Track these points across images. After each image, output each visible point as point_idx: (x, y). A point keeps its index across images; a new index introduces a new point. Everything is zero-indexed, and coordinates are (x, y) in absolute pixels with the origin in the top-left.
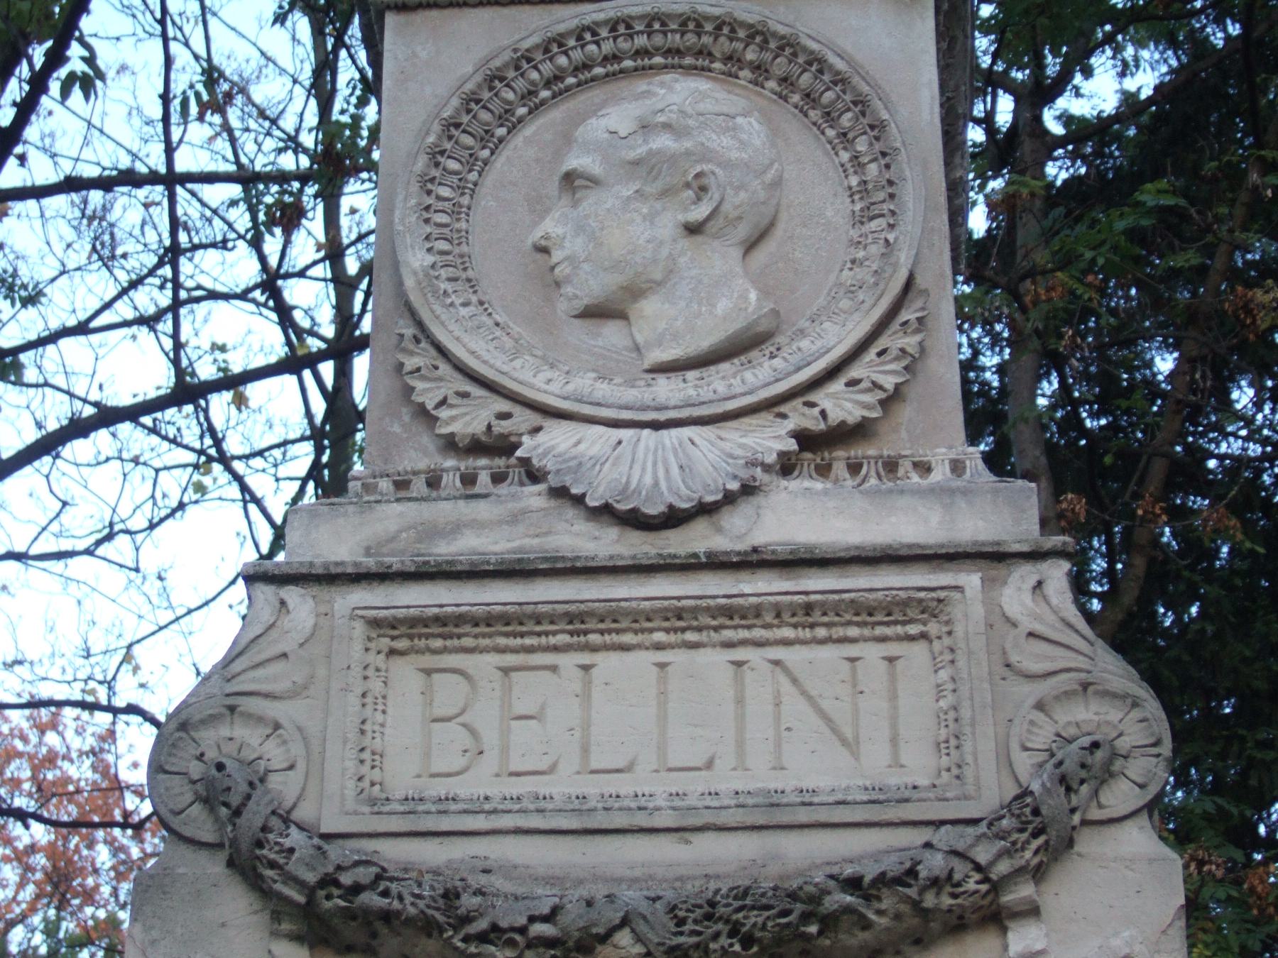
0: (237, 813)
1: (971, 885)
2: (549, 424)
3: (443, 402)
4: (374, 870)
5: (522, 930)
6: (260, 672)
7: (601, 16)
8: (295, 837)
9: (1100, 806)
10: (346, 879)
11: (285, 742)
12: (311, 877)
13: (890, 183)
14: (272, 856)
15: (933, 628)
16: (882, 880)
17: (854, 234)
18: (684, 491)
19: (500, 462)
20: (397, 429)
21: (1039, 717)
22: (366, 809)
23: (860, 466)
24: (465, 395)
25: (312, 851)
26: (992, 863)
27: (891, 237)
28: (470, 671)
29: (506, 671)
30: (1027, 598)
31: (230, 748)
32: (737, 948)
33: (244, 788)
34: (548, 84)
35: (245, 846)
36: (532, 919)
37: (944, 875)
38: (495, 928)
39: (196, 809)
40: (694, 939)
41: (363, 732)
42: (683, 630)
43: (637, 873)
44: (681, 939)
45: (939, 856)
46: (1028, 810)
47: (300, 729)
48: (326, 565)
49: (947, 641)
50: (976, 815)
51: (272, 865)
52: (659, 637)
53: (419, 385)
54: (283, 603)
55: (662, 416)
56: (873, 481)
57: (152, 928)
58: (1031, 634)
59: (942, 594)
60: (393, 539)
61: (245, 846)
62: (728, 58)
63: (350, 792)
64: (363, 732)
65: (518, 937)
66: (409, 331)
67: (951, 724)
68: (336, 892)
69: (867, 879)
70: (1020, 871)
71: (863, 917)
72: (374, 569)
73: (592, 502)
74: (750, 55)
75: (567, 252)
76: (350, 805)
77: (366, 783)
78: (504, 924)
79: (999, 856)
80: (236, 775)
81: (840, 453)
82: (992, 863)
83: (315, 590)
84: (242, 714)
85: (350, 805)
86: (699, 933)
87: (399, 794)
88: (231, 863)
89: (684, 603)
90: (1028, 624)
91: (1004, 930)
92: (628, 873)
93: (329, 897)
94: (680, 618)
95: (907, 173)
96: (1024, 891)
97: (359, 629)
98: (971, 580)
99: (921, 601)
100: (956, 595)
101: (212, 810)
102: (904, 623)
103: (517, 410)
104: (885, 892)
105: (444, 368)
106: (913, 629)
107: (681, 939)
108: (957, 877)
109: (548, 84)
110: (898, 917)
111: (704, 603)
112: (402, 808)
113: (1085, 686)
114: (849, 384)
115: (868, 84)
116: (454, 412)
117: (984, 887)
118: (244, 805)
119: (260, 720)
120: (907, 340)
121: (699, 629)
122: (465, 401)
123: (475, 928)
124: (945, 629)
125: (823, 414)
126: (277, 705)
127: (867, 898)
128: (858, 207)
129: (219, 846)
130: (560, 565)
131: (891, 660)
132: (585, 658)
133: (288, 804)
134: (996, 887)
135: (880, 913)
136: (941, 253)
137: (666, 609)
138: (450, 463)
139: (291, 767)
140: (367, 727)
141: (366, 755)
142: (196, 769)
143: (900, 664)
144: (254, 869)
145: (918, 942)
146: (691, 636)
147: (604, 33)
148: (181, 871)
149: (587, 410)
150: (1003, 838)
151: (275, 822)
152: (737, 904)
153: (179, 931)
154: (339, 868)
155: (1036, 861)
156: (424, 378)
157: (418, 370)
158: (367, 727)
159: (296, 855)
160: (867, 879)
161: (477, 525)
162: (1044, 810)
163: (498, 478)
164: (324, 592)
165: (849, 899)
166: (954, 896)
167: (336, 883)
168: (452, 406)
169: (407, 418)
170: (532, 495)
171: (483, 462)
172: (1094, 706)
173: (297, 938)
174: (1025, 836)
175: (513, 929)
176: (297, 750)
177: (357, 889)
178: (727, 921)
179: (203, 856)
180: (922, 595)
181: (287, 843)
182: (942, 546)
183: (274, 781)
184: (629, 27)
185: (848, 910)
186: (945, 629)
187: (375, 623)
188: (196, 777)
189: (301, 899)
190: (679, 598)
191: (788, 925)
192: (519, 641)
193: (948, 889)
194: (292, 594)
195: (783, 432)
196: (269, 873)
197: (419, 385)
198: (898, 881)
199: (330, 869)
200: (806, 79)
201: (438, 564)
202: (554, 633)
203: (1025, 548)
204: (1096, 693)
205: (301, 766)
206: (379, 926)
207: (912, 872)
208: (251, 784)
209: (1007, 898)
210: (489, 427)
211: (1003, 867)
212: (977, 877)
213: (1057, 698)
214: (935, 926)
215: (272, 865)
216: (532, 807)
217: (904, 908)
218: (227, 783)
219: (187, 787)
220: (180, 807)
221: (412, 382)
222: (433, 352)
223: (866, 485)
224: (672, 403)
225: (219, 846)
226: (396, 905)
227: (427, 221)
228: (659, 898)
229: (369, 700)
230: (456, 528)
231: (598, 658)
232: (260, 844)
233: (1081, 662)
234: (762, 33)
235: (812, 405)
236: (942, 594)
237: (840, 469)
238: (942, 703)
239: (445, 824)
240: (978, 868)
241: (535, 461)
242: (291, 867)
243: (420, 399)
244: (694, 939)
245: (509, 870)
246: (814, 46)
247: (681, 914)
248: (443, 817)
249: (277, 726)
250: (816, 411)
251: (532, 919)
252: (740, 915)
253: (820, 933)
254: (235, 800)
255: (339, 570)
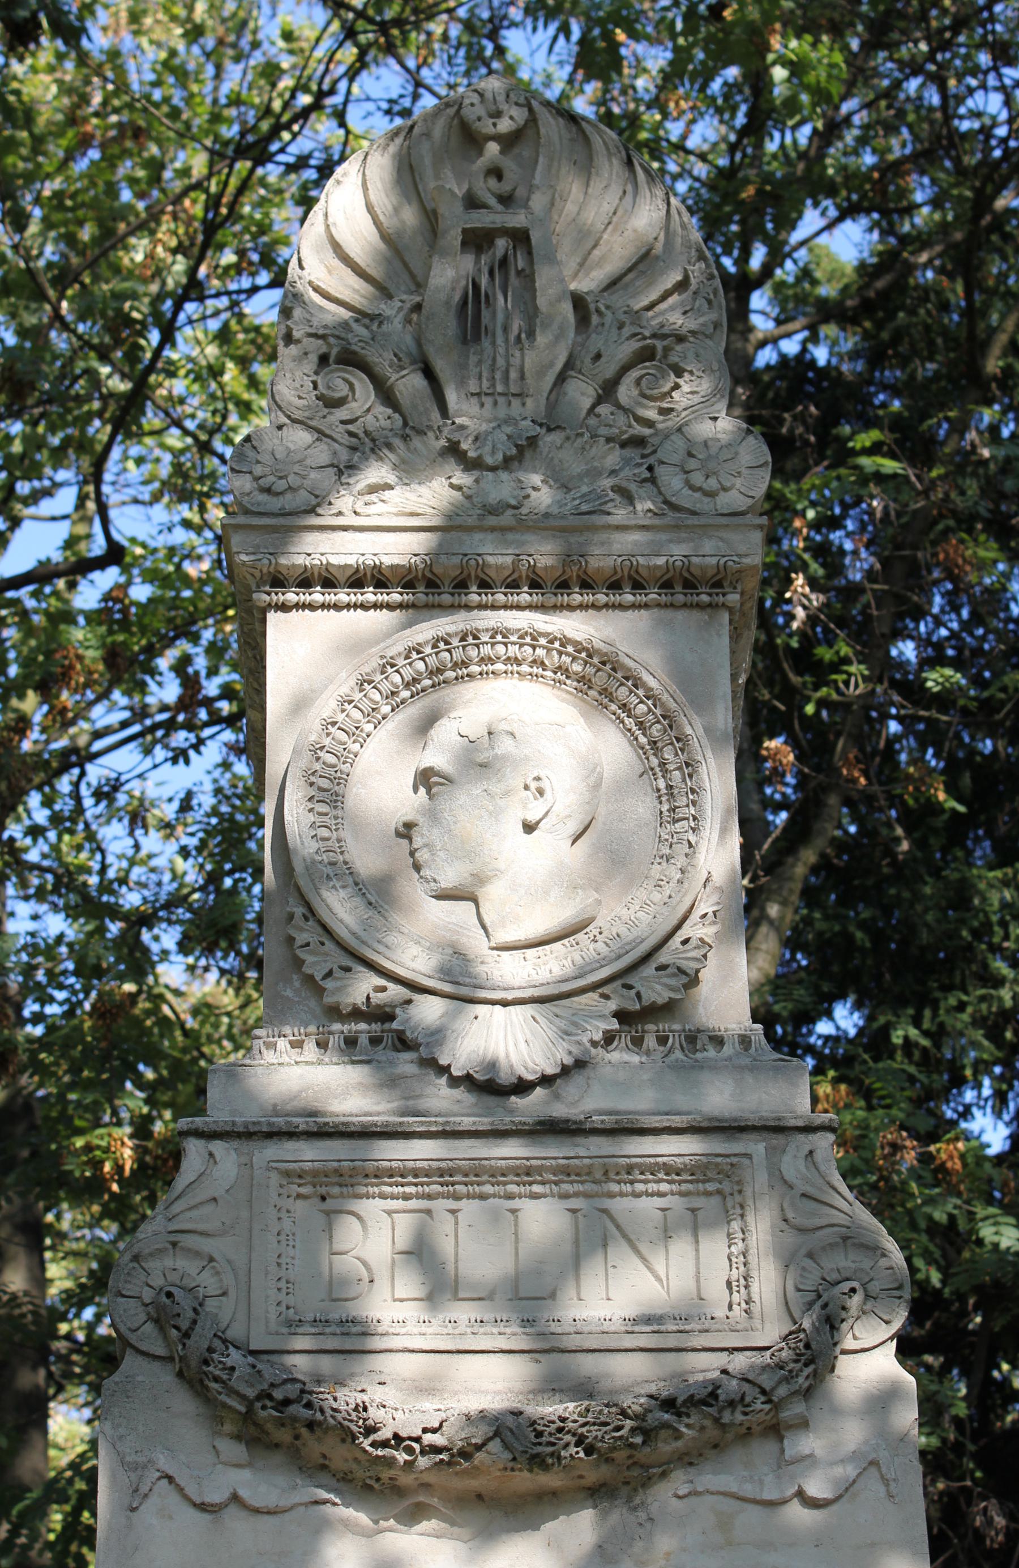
0: (187, 1335)
1: (758, 1406)
2: (417, 997)
3: (330, 974)
4: (298, 1386)
5: (418, 1440)
6: (195, 1213)
7: (451, 629)
8: (235, 1357)
9: (855, 1338)
10: (278, 1394)
11: (218, 1273)
12: (251, 1393)
13: (693, 791)
14: (217, 1373)
16: (692, 1401)
18: (531, 1065)
20: (289, 993)
21: (808, 1263)
22: (285, 1330)
23: (667, 1038)
25: (249, 1370)
26: (773, 1389)
27: (693, 839)
29: (389, 1213)
30: (801, 1164)
31: (173, 1278)
32: (582, 1455)
33: (190, 1314)
34: (407, 685)
35: (194, 1363)
36: (425, 1430)
37: (738, 1398)
38: (396, 1436)
39: (149, 1327)
40: (551, 1449)
41: (279, 1264)
42: (530, 1184)
44: (539, 1449)
45: (734, 1382)
46: (801, 1345)
47: (229, 1262)
48: (246, 1125)
49: (738, 1198)
51: (216, 1379)
52: (513, 1188)
53: (309, 959)
54: (211, 1155)
55: (510, 996)
56: (678, 1054)
57: (119, 1425)
58: (803, 1195)
59: (734, 1160)
61: (194, 1363)
62: (559, 669)
63: (273, 1317)
64: (279, 1264)
65: (416, 1446)
66: (299, 911)
67: (742, 1268)
68: (269, 1404)
69: (680, 1401)
70: (795, 1393)
71: (676, 1430)
72: (285, 1129)
73: (456, 1072)
74: (577, 667)
75: (425, 840)
76: (273, 1327)
77: (283, 1308)
78: (404, 1434)
79: (779, 1383)
80: (183, 1303)
81: (651, 1027)
82: (773, 1389)
83: (235, 1143)
84: (183, 1249)
85: (273, 1327)
86: (553, 1444)
87: (310, 1317)
88: (180, 1374)
89: (534, 1162)
90: (802, 1187)
91: (781, 1439)
93: (264, 1408)
94: (528, 1174)
95: (689, 731)
96: (797, 1408)
97: (275, 1178)
98: (757, 1147)
99: (717, 1164)
100: (746, 1161)
101: (162, 1329)
102: (704, 1182)
103: (391, 986)
104: (693, 1411)
105: (329, 945)
106: (711, 1187)
107: (539, 1449)
108: (748, 1399)
109: (407, 685)
110: (703, 1428)
111: (547, 1163)
112: (313, 1330)
113: (845, 1239)
114: (658, 969)
117: (767, 1407)
118: (192, 1329)
119: (197, 1254)
120: (705, 930)
121: (543, 1183)
123: (378, 1436)
124: (736, 1188)
125: (638, 995)
126: (210, 1241)
127: (679, 1415)
130: (433, 1129)
131: (693, 1210)
132: (452, 1204)
133: (223, 1325)
134: (777, 1406)
135: (688, 1426)
137: (518, 1167)
139: (224, 1294)
140: (283, 1260)
141: (282, 1284)
142: (148, 1295)
143: (700, 1213)
144: (201, 1381)
145: (715, 1446)
146: (537, 1188)
147: (455, 642)
148: (140, 1378)
150: (782, 1368)
151: (217, 1344)
152: (582, 1420)
153: (141, 1428)
154: (272, 1385)
155: (806, 1384)
156: (313, 953)
157: (308, 945)
158: (283, 1260)
159: (237, 1374)
160: (680, 1401)
162: (814, 1345)
163: (375, 1041)
164: (245, 1146)
165: (666, 1416)
166: (745, 1414)
167: (270, 1397)
169: (297, 984)
170: (406, 1062)
171: (363, 1026)
172: (852, 1256)
173: (238, 1437)
174: (799, 1365)
175: (411, 1439)
176: (228, 1280)
177: (287, 1402)
178: (574, 1435)
179: (156, 1365)
180: (719, 1160)
181: (229, 1362)
182: (735, 1120)
183: (211, 1305)
184: (475, 637)
185: (666, 1425)
186: (736, 1188)
187: (287, 1174)
188: (148, 1301)
189: (242, 1409)
190: (528, 1159)
191: (621, 1438)
192: (400, 1189)
193: (740, 1408)
194: (218, 1147)
195: (607, 1012)
196: (213, 1385)
198: (704, 1402)
199: (266, 1386)
200: (623, 692)
201: (336, 1126)
202: (428, 1184)
203: (800, 1123)
204: (854, 1245)
205: (232, 1293)
207: (713, 1395)
208: (195, 1310)
209: (785, 1414)
210: (368, 998)
211: (782, 1391)
212: (763, 1399)
213: (823, 1249)
214: (730, 1436)
215: (216, 1379)
216: (416, 1330)
217: (708, 1423)
218: (176, 1310)
219: (141, 1308)
220: (136, 1325)
221: (301, 954)
222: (320, 930)
223: (672, 1057)
224: (517, 984)
225: (170, 1359)
226: (319, 1416)
227: (311, 810)
229: (283, 1237)
231: (464, 1203)
232: (206, 1362)
234: (587, 650)
235: (630, 987)
236: (734, 1160)
237: (650, 1041)
238: (733, 1249)
240: (763, 1392)
241: (408, 1034)
242: (233, 1383)
243: (309, 971)
244: (551, 1449)
246: (631, 664)
247: (540, 1428)
248: (346, 1338)
249: (211, 1260)
250: (633, 992)
251: (425, 1430)
252: (584, 1430)
253: (644, 1442)
254: (185, 1325)
255: (256, 1129)
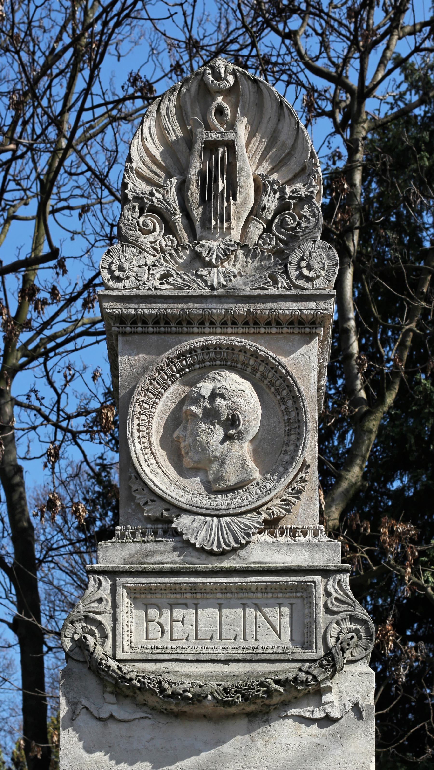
15: (305, 595)
17: (286, 439)
19: (165, 526)
24: (153, 501)
28: (160, 605)
43: (213, 674)
50: (315, 658)
55: (220, 513)
60: (133, 556)
88: (90, 668)
92: (210, 674)
96: (329, 684)
115: (293, 380)
116: (150, 507)
122: (154, 503)
128: (287, 429)
129: (85, 662)
136: (313, 563)
138: (149, 526)
149: (195, 509)
156: (139, 494)
157: (137, 490)
161: (160, 552)
168: (149, 505)
171: (160, 526)
197: (138, 496)
204: (385, 102)
206: (137, 691)
228: (221, 685)
230: (153, 553)
233: (350, 608)
239: (155, 657)
243: (138, 502)
245: (175, 673)
